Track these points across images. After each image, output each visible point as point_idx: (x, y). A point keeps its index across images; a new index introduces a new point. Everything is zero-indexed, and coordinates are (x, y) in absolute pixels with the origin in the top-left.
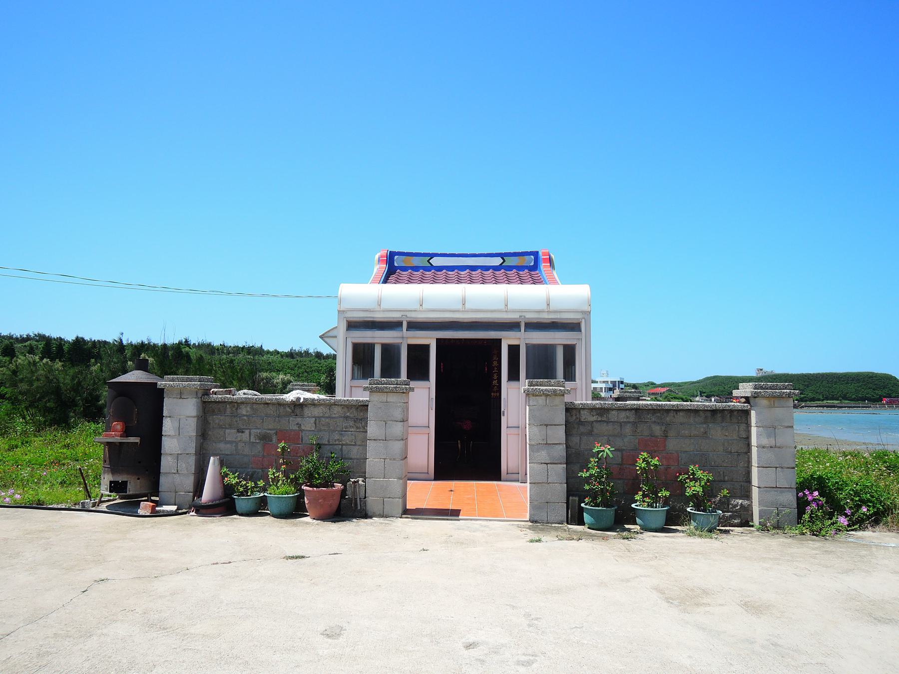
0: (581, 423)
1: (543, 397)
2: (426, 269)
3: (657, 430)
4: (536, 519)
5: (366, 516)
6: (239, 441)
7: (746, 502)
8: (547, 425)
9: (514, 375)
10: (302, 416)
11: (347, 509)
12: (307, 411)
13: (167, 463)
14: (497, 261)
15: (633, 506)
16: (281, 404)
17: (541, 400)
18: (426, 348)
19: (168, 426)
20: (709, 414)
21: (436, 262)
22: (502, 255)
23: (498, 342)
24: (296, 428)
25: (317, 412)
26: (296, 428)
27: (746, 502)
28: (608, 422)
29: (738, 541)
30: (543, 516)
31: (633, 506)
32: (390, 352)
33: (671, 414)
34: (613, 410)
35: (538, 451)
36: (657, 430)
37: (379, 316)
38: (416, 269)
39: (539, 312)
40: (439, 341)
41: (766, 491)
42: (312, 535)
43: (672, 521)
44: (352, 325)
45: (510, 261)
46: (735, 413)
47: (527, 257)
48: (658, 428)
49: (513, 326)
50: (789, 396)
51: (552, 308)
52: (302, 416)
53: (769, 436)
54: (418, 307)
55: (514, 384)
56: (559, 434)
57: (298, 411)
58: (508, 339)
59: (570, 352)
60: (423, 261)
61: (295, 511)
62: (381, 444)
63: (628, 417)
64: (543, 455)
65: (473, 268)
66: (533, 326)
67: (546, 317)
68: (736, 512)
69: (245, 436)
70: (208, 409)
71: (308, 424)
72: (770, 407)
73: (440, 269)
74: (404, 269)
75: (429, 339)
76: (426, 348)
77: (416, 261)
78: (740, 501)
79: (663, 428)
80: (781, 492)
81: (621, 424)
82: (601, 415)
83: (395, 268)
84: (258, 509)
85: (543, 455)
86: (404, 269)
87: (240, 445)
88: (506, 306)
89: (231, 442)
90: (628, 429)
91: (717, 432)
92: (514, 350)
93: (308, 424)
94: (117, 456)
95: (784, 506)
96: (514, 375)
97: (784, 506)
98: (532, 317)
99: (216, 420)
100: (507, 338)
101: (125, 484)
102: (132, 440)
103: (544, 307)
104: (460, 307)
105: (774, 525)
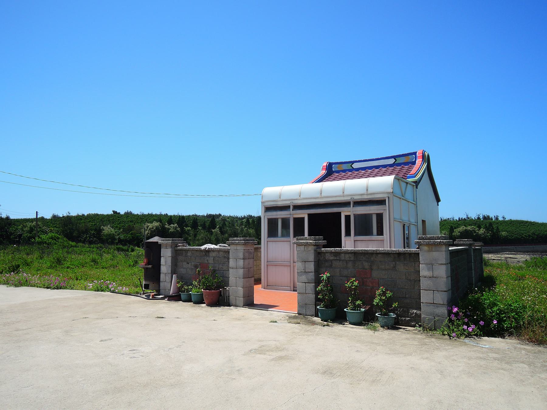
0: (326, 261)
1: (303, 247)
2: (350, 170)
3: (366, 265)
4: (300, 312)
5: (229, 305)
6: (186, 268)
7: (418, 312)
8: (305, 262)
9: (348, 234)
10: (209, 256)
11: (220, 300)
12: (211, 254)
13: (162, 276)
14: (392, 161)
15: (345, 310)
16: (201, 251)
17: (302, 248)
18: (303, 218)
19: (163, 260)
20: (396, 256)
21: (355, 166)
22: (394, 157)
23: (339, 214)
24: (207, 262)
25: (214, 254)
26: (207, 262)
27: (418, 312)
28: (340, 260)
29: (405, 337)
30: (303, 311)
31: (345, 310)
32: (285, 222)
33: (374, 256)
34: (342, 253)
35: (301, 276)
36: (366, 265)
37: (280, 204)
38: (344, 171)
39: (362, 195)
40: (310, 215)
41: (427, 306)
42: (203, 311)
43: (366, 320)
44: (268, 209)
45: (400, 160)
46: (413, 255)
47: (410, 157)
48: (367, 264)
49: (346, 204)
50: (310, 244)
51: (323, 195)
52: (209, 256)
53: (429, 270)
54: (298, 197)
55: (348, 238)
56: (311, 267)
57: (207, 254)
58: (345, 212)
59: (380, 217)
60: (347, 167)
61: (199, 301)
62: (235, 270)
63: (350, 258)
64: (304, 278)
65: (377, 167)
66: (358, 203)
67: (366, 197)
68: (413, 317)
69: (190, 265)
70: (177, 254)
71: (211, 261)
72: (429, 251)
73: (357, 170)
74: (338, 172)
75: (304, 214)
76: (303, 218)
77: (344, 167)
78: (415, 311)
79: (369, 264)
80: (437, 307)
81: (347, 262)
82: (335, 256)
83: (331, 172)
84: (189, 300)
85: (304, 278)
86: (338, 172)
87: (188, 269)
88: (367, 190)
89: (185, 268)
90: (350, 265)
91: (401, 267)
92: (348, 218)
93: (211, 261)
94: (139, 271)
95: (439, 316)
96: (348, 234)
97: (439, 316)
98: (357, 198)
99: (180, 258)
100: (344, 212)
101: (148, 285)
102: (150, 266)
103: (364, 192)
104: (319, 195)
105: (431, 328)
